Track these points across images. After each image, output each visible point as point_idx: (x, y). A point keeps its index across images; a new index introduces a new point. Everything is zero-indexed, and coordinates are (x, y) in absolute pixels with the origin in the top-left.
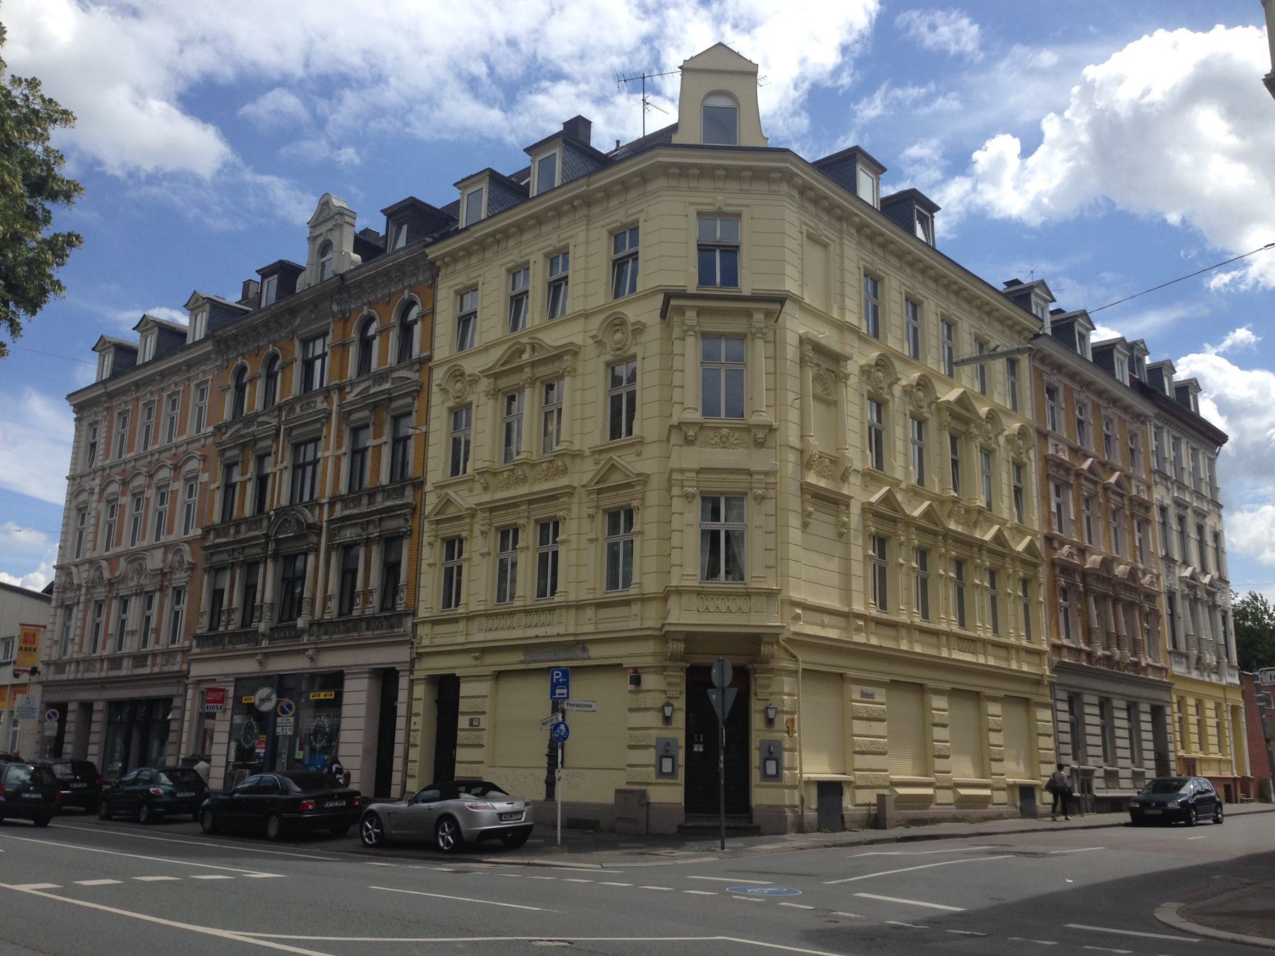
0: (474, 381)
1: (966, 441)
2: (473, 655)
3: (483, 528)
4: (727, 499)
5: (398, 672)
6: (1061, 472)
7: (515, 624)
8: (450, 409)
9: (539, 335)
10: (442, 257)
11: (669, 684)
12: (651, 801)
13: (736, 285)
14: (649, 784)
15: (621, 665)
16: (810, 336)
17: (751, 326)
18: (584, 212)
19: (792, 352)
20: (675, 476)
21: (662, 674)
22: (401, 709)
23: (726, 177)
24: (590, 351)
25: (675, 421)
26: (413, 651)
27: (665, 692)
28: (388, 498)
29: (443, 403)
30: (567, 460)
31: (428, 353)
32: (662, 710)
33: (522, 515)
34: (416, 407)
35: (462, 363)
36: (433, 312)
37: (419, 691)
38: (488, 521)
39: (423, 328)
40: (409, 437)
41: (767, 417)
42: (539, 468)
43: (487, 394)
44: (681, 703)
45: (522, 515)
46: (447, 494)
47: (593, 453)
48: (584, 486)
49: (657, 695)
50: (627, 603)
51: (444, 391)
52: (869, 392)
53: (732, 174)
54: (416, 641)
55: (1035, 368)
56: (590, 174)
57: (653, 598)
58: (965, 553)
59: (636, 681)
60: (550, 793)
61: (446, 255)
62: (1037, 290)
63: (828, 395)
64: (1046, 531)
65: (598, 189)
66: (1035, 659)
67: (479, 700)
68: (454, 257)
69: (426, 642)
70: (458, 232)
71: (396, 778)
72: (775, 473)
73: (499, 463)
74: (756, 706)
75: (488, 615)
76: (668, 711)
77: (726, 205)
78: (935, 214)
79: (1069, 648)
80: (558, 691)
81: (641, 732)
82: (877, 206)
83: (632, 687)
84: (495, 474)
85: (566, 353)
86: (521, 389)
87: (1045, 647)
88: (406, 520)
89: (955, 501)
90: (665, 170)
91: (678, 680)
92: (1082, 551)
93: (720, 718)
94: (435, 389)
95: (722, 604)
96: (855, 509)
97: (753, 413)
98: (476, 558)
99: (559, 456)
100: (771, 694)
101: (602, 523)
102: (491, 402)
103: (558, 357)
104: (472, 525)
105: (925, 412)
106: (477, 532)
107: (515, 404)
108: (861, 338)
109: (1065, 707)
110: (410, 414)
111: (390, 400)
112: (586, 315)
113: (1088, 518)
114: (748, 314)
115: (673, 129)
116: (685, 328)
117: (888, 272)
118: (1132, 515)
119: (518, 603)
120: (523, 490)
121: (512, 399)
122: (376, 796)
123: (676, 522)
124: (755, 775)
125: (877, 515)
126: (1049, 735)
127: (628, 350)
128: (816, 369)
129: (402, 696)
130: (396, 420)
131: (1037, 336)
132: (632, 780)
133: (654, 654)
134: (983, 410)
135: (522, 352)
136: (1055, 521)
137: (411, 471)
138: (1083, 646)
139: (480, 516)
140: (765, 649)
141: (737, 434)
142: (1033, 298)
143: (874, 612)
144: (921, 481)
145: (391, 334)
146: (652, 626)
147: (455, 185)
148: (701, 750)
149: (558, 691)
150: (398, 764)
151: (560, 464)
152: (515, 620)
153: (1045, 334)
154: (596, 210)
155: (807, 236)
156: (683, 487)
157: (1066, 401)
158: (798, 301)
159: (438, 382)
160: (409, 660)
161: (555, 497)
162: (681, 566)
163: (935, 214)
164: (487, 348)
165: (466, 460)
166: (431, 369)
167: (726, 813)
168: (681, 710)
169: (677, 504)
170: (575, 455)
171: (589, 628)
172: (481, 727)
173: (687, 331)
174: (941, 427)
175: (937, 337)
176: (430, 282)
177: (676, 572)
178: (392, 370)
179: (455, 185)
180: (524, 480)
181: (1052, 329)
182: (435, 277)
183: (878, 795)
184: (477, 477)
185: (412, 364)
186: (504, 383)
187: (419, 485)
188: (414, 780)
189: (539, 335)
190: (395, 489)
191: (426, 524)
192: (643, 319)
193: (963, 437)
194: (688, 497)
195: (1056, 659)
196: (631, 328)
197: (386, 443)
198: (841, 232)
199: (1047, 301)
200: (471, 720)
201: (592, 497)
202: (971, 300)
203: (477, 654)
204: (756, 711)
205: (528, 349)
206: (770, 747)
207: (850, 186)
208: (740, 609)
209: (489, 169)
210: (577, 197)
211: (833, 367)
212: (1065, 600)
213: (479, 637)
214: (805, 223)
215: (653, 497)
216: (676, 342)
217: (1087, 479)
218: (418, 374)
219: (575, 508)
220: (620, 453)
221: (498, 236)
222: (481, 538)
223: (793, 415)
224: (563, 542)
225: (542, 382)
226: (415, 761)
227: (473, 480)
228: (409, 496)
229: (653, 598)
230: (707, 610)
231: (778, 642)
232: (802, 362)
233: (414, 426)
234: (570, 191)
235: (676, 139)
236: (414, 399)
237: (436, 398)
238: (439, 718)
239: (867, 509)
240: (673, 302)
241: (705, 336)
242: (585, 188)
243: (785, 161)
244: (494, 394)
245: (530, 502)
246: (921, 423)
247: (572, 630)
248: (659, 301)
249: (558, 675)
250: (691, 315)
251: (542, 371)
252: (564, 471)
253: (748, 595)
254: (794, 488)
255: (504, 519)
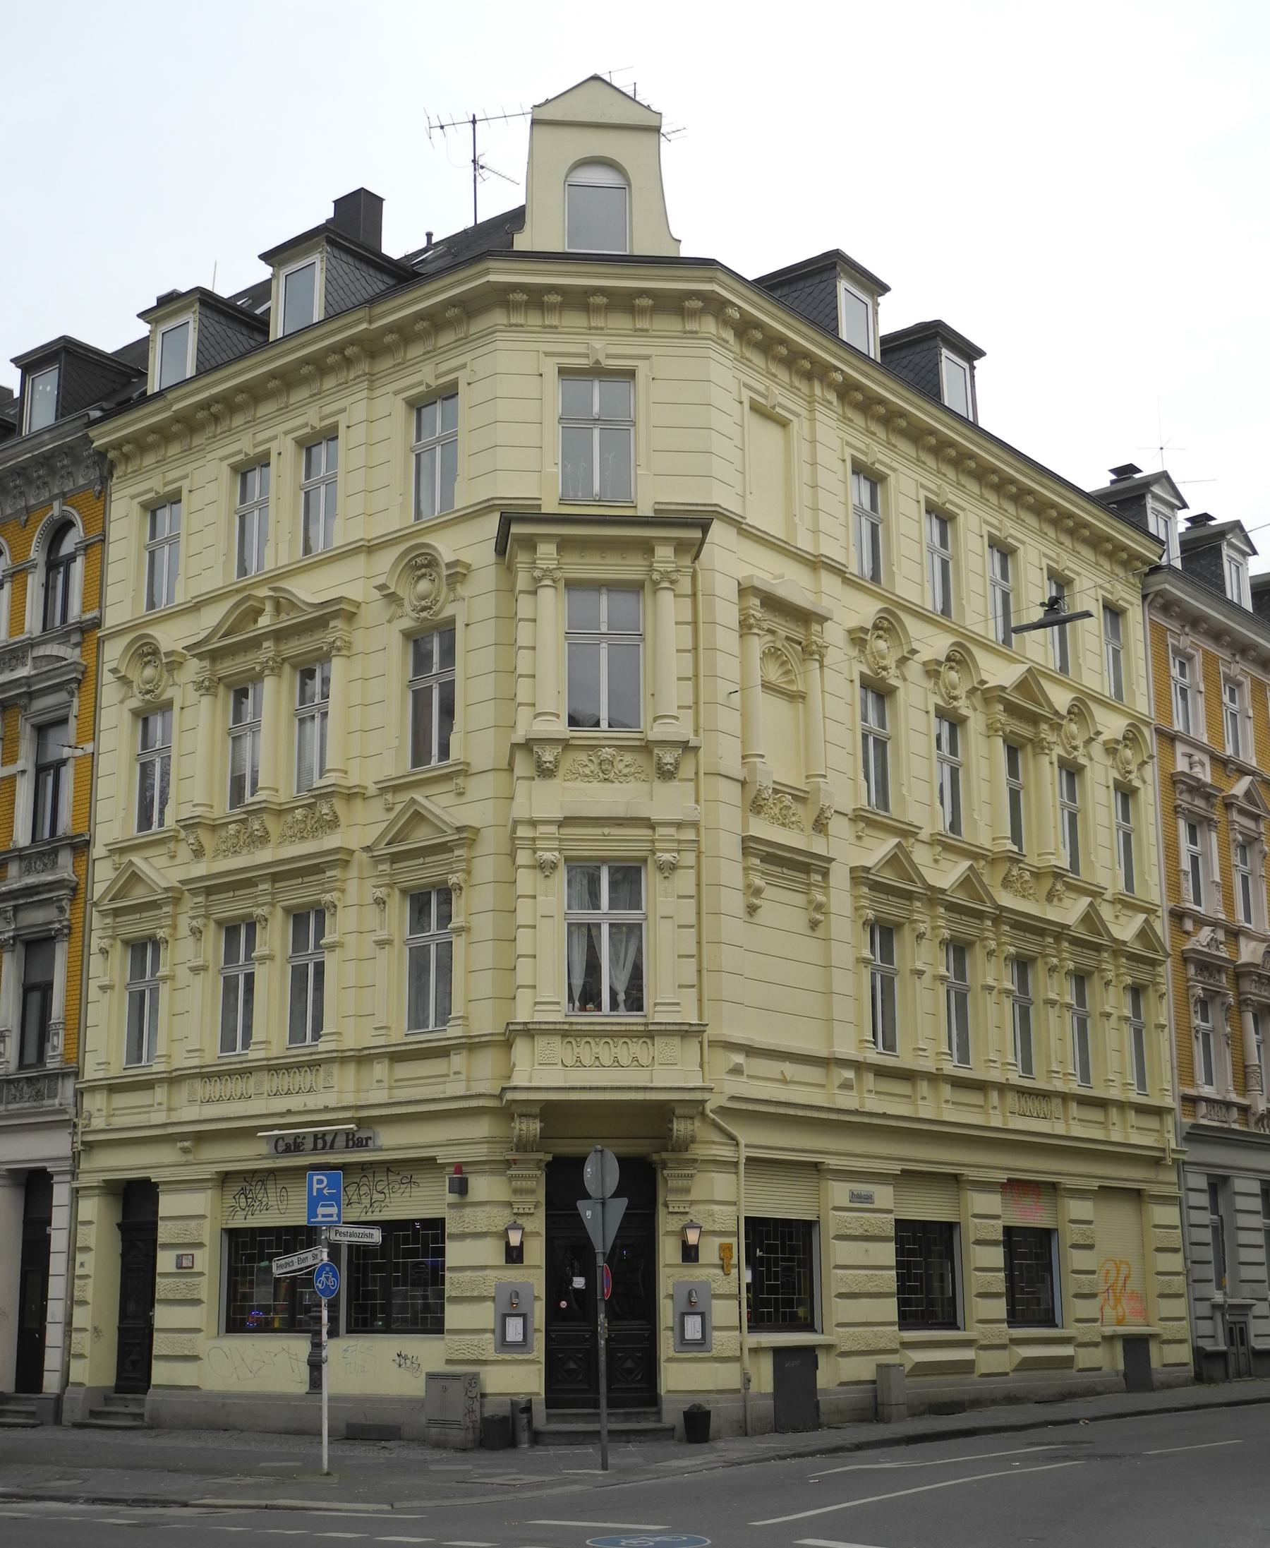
0: (174, 664)
1: (1035, 755)
2: (179, 1145)
3: (194, 923)
4: (613, 872)
5: (50, 1176)
6: (1200, 802)
7: (251, 1091)
8: (136, 713)
9: (283, 584)
10: (117, 445)
11: (516, 1191)
12: (489, 1389)
13: (348, 1331)
14: (484, 1362)
15: (433, 1159)
16: (757, 583)
17: (651, 569)
18: (364, 367)
19: (727, 613)
20: (522, 832)
21: (503, 1173)
22: (58, 1241)
23: (608, 309)
24: (375, 609)
25: (519, 736)
26: (79, 1138)
27: (510, 1204)
28: (28, 871)
29: (122, 702)
30: (339, 805)
31: (95, 613)
32: (504, 1235)
33: (261, 900)
34: (75, 710)
35: (155, 632)
36: (103, 540)
37: (90, 1208)
38: (202, 911)
39: (87, 568)
40: (64, 762)
41: (682, 729)
42: (289, 818)
43: (199, 686)
44: (537, 1223)
45: (261, 900)
46: (131, 863)
47: (383, 791)
48: (368, 849)
49: (494, 1211)
50: (442, 1052)
51: (124, 681)
52: (862, 675)
53: (623, 302)
54: (81, 1122)
55: (1152, 622)
56: (372, 301)
57: (487, 1044)
58: (1030, 945)
59: (461, 1187)
60: (316, 1383)
61: (127, 440)
62: (1156, 489)
63: (791, 682)
64: (1172, 904)
65: (389, 329)
66: (1153, 1123)
67: (193, 1223)
68: (140, 444)
69: (98, 1123)
70: (145, 399)
71: (52, 1359)
72: (695, 825)
73: (221, 808)
74: (666, 1224)
75: (205, 1075)
76: (515, 1239)
77: (608, 356)
78: (976, 363)
79: (1208, 1100)
80: (321, 1211)
81: (468, 1273)
82: (874, 352)
83: (452, 1198)
84: (214, 828)
85: (335, 615)
86: (257, 678)
87: (1169, 1101)
88: (61, 910)
89: (1014, 860)
90: (501, 297)
91: (530, 1184)
92: (1234, 934)
93: (599, 1249)
94: (107, 677)
95: (605, 1051)
96: (839, 877)
97: (656, 719)
98: (183, 973)
99: (327, 795)
100: (692, 1203)
101: (399, 913)
102: (206, 701)
103: (321, 623)
104: (174, 917)
105: (963, 707)
106: (183, 929)
107: (249, 703)
108: (847, 581)
109: (1204, 1200)
110: (64, 721)
111: (31, 696)
112: (370, 549)
113: (1245, 879)
114: (646, 547)
115: (516, 218)
116: (537, 573)
117: (895, 465)
118: (1242, 1003)
119: (255, 1054)
120: (264, 855)
121: (241, 694)
122: (17, 1391)
123: (525, 913)
124: (666, 1344)
125: (876, 887)
126: (1176, 1250)
127: (161, 694)
128: (769, 637)
129: (59, 1217)
130: (41, 730)
131: (1156, 569)
132: (454, 1357)
133: (489, 1141)
134: (1061, 699)
135: (259, 612)
136: (1187, 886)
137: (66, 823)
138: (1234, 1097)
139: (189, 901)
140: (680, 1128)
141: (628, 758)
142: (1150, 503)
143: (873, 1056)
144: (955, 826)
145: (30, 578)
146: (482, 1090)
147: (140, 316)
148: (564, 1302)
149: (321, 1211)
150: (54, 1335)
151: (325, 811)
152: (250, 1084)
153: (1170, 567)
154: (386, 363)
155: (751, 408)
156: (535, 851)
157: (1206, 678)
158: (736, 523)
159: (113, 665)
160: (70, 1154)
161: (317, 869)
162: (534, 987)
163: (976, 363)
164: (196, 607)
165: (164, 802)
166: (100, 642)
167: (610, 1405)
168: (537, 1234)
169: (526, 881)
170: (351, 796)
171: (380, 1096)
172: (195, 1270)
173: (540, 580)
174: (991, 730)
175: (984, 576)
176: (98, 488)
177: (524, 997)
178: (32, 644)
179: (140, 316)
180: (264, 839)
181: (1183, 560)
182: (105, 479)
183: (879, 1366)
184: (183, 834)
185: (68, 634)
186: (229, 667)
187: (81, 846)
188: (82, 1362)
189: (283, 584)
190: (42, 854)
191: (95, 914)
192: (466, 557)
193: (1029, 748)
194: (545, 868)
195: (1188, 1121)
196: (445, 572)
197: (23, 772)
198: (811, 400)
199: (1173, 507)
200: (179, 1257)
201: (381, 867)
202: (1040, 509)
203: (187, 1144)
204: (668, 1233)
205: (269, 607)
206: (690, 1294)
207: (826, 324)
208: (635, 1059)
209: (199, 290)
210: (351, 341)
211: (798, 633)
212: (1205, 1019)
213: (190, 1113)
214: (746, 386)
215: (486, 867)
216: (522, 598)
217: (1243, 812)
218: (77, 651)
219: (352, 887)
220: (430, 790)
221: (215, 409)
222: (191, 939)
223: (728, 720)
224: (332, 947)
225: (294, 667)
226: (84, 1330)
227: (175, 839)
228: (65, 867)
229: (487, 1044)
230: (579, 1064)
231: (703, 1114)
232: (745, 627)
233: (72, 743)
234: (340, 330)
235: (522, 242)
236: (71, 694)
237: (110, 692)
238: (124, 1256)
239: (859, 876)
240: (515, 529)
241: (571, 585)
242: (364, 326)
243: (711, 280)
244: (207, 687)
245: (275, 878)
246: (955, 722)
247: (349, 1100)
248: (491, 524)
249: (320, 1182)
250: (547, 551)
251: (295, 647)
252: (333, 823)
253: (648, 1034)
254: (730, 847)
255: (231, 908)
